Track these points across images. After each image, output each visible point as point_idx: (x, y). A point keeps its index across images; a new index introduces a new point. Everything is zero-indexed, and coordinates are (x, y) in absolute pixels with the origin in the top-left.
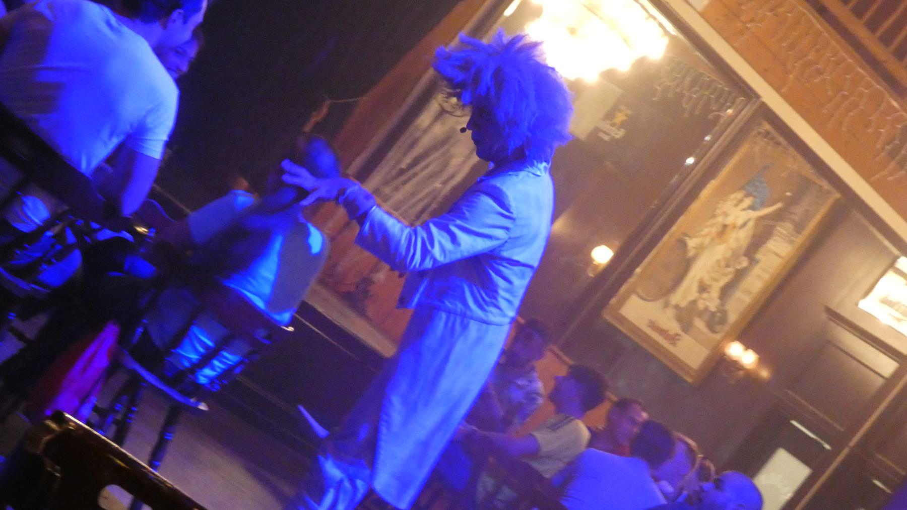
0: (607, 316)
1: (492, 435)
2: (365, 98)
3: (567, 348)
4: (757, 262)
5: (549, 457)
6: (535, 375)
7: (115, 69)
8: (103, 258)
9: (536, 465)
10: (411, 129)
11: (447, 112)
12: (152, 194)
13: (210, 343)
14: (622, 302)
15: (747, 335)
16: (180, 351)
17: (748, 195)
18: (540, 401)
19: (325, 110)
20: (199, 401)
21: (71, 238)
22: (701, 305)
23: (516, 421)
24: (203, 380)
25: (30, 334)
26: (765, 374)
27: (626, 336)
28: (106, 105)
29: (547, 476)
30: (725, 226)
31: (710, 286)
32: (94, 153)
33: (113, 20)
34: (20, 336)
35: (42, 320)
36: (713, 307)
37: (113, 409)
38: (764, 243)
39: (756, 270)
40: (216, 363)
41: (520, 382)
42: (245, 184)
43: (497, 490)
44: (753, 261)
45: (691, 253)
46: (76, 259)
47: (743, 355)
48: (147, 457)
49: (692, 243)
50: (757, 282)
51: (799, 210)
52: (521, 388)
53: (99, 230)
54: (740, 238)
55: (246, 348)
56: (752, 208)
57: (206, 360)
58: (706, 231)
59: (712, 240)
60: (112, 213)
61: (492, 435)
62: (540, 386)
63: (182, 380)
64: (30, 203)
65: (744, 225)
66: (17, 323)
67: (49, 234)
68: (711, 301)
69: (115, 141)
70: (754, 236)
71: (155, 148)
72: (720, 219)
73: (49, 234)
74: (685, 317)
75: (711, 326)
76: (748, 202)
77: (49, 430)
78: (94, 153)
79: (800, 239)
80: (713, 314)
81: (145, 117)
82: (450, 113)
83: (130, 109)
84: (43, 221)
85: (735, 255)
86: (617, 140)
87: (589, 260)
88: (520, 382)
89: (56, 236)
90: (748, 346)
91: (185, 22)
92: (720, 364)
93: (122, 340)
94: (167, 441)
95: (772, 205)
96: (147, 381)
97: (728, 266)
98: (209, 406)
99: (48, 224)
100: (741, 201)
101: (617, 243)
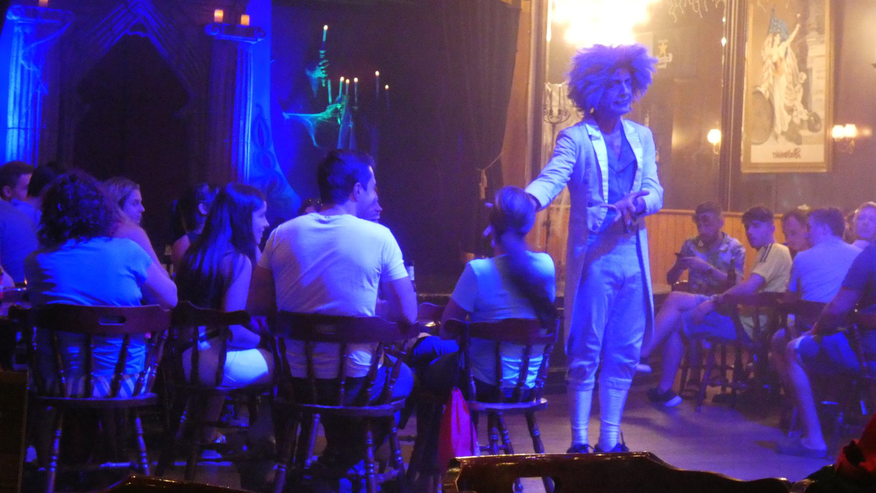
0: (745, 170)
1: (729, 291)
2: (502, 153)
3: (735, 208)
4: (811, 69)
5: (775, 277)
6: (729, 237)
7: (343, 246)
8: (421, 357)
9: (770, 289)
10: (543, 149)
11: (558, 123)
12: (419, 300)
13: (520, 361)
14: (748, 156)
15: (838, 116)
16: (505, 378)
17: (775, 35)
18: (743, 250)
19: (485, 177)
20: (538, 399)
21: (394, 359)
22: (797, 121)
23: (737, 272)
24: (531, 385)
25: (414, 433)
26: (867, 132)
27: (765, 174)
28: (357, 271)
29: (782, 290)
30: (775, 64)
31: (794, 106)
32: (368, 301)
33: (323, 218)
34: (409, 439)
35: (413, 421)
36: (805, 117)
37: (492, 442)
38: (806, 55)
39: (814, 75)
40: (530, 369)
41: (722, 249)
42: (472, 255)
43: (757, 322)
44: (807, 71)
45: (767, 96)
46: (407, 370)
47: (846, 131)
48: (533, 450)
49: (763, 89)
50: (820, 82)
51: (812, 20)
52: (725, 252)
53: (406, 341)
54: (791, 62)
55: (541, 348)
56: (783, 40)
57: (524, 372)
58: (766, 75)
59: (774, 77)
60: (409, 329)
61: (729, 291)
62: (736, 241)
63: (519, 393)
64: (355, 357)
65: (786, 54)
66: (401, 433)
67: (379, 366)
68: (802, 114)
69: (376, 285)
70: (797, 56)
71: (400, 271)
72: (769, 62)
73: (379, 366)
74: (793, 135)
75: (812, 127)
76: (778, 39)
77: (456, 474)
78: (368, 301)
79: (827, 36)
80: (809, 121)
81: (382, 258)
82: (558, 123)
83: (371, 262)
84: (371, 362)
85: (795, 76)
86: (672, 63)
87: (710, 146)
88: (722, 249)
89: (384, 364)
90: (843, 123)
91: (365, 189)
92: (835, 148)
93: (467, 396)
94: (538, 437)
95: (793, 31)
96: (500, 410)
97: (795, 85)
98: (546, 398)
99: (375, 361)
100: (773, 41)
101: (718, 123)
